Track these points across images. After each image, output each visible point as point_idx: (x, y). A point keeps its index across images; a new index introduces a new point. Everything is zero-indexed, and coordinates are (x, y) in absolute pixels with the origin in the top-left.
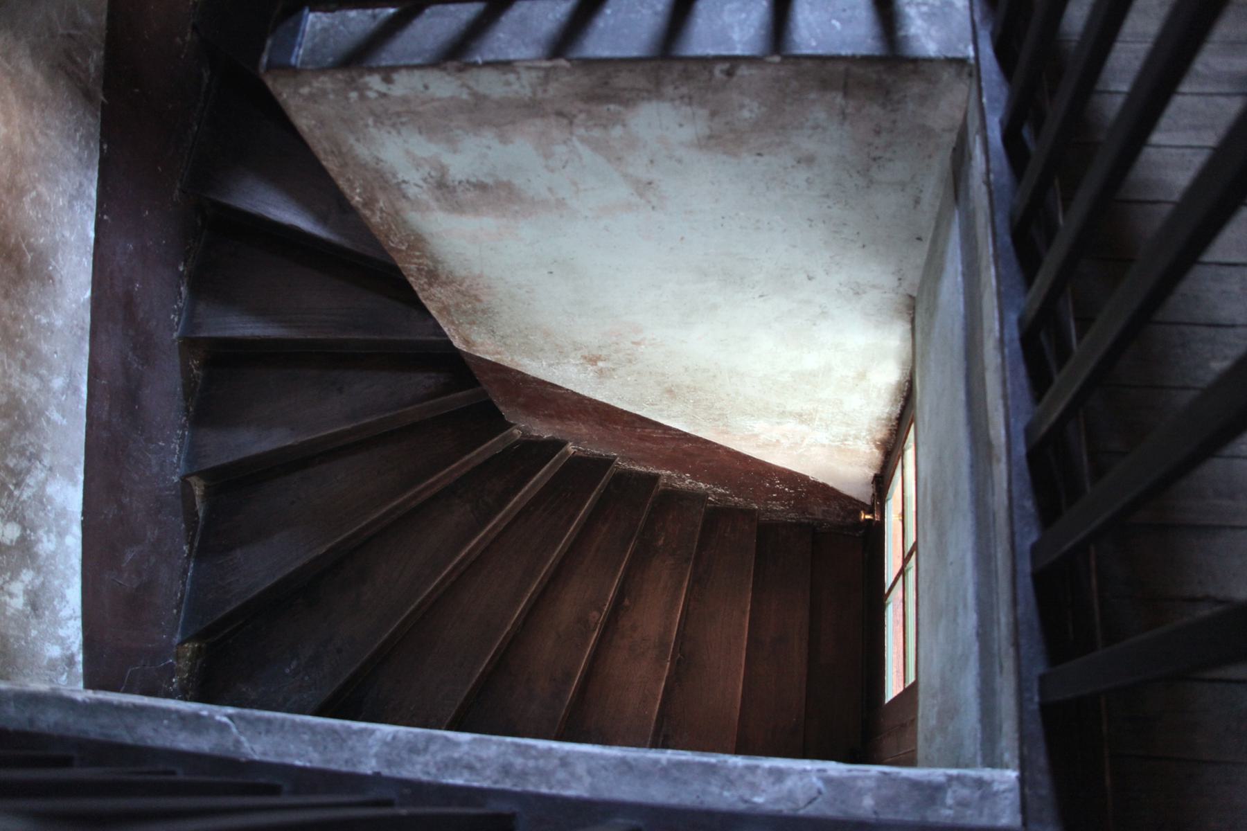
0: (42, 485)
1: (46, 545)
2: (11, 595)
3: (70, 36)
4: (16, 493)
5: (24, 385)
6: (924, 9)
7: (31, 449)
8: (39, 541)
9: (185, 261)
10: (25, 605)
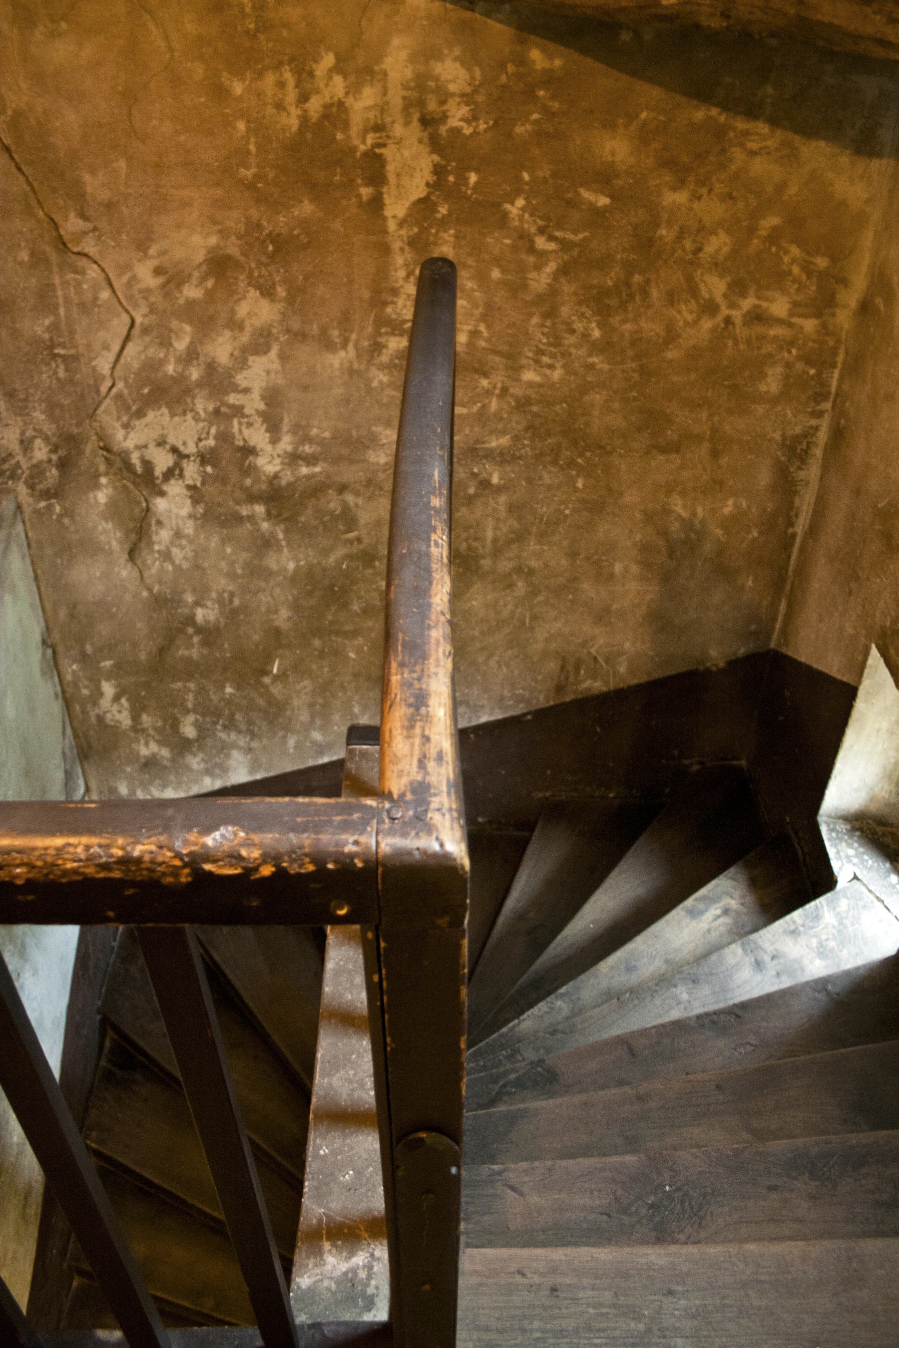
0: (234, 746)
1: (195, 762)
2: (147, 744)
3: (595, 659)
4: (219, 727)
5: (299, 709)
6: (362, 1274)
7: (256, 729)
8: (195, 755)
9: (490, 822)
10: (145, 757)
